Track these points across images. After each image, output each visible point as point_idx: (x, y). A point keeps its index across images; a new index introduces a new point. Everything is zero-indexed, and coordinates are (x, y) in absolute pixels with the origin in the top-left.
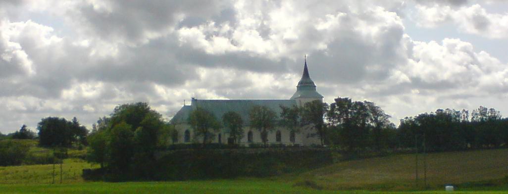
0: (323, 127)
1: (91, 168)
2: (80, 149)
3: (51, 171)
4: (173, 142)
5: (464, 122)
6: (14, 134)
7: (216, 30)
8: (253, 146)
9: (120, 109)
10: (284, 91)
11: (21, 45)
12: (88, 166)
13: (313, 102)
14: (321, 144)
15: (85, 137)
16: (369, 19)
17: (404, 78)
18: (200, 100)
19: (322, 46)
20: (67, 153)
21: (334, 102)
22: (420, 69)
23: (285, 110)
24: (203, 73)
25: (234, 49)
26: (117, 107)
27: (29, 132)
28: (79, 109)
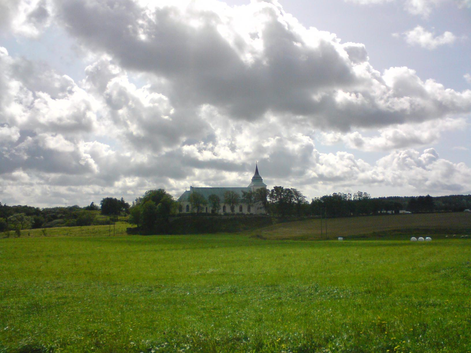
0: (267, 203)
1: (131, 227)
2: (125, 216)
3: (108, 229)
4: (180, 212)
5: (349, 200)
6: (86, 207)
7: (204, 146)
8: (226, 214)
9: (148, 193)
10: (244, 182)
11: (91, 155)
12: (130, 226)
13: (261, 189)
14: (265, 213)
15: (128, 209)
16: (294, 140)
17: (314, 174)
18: (195, 188)
19: (266, 156)
20: (117, 219)
21: (273, 188)
22: (323, 169)
23: (245, 194)
24: (197, 172)
25: (215, 157)
26: (147, 192)
27: (95, 206)
28: (125, 193)
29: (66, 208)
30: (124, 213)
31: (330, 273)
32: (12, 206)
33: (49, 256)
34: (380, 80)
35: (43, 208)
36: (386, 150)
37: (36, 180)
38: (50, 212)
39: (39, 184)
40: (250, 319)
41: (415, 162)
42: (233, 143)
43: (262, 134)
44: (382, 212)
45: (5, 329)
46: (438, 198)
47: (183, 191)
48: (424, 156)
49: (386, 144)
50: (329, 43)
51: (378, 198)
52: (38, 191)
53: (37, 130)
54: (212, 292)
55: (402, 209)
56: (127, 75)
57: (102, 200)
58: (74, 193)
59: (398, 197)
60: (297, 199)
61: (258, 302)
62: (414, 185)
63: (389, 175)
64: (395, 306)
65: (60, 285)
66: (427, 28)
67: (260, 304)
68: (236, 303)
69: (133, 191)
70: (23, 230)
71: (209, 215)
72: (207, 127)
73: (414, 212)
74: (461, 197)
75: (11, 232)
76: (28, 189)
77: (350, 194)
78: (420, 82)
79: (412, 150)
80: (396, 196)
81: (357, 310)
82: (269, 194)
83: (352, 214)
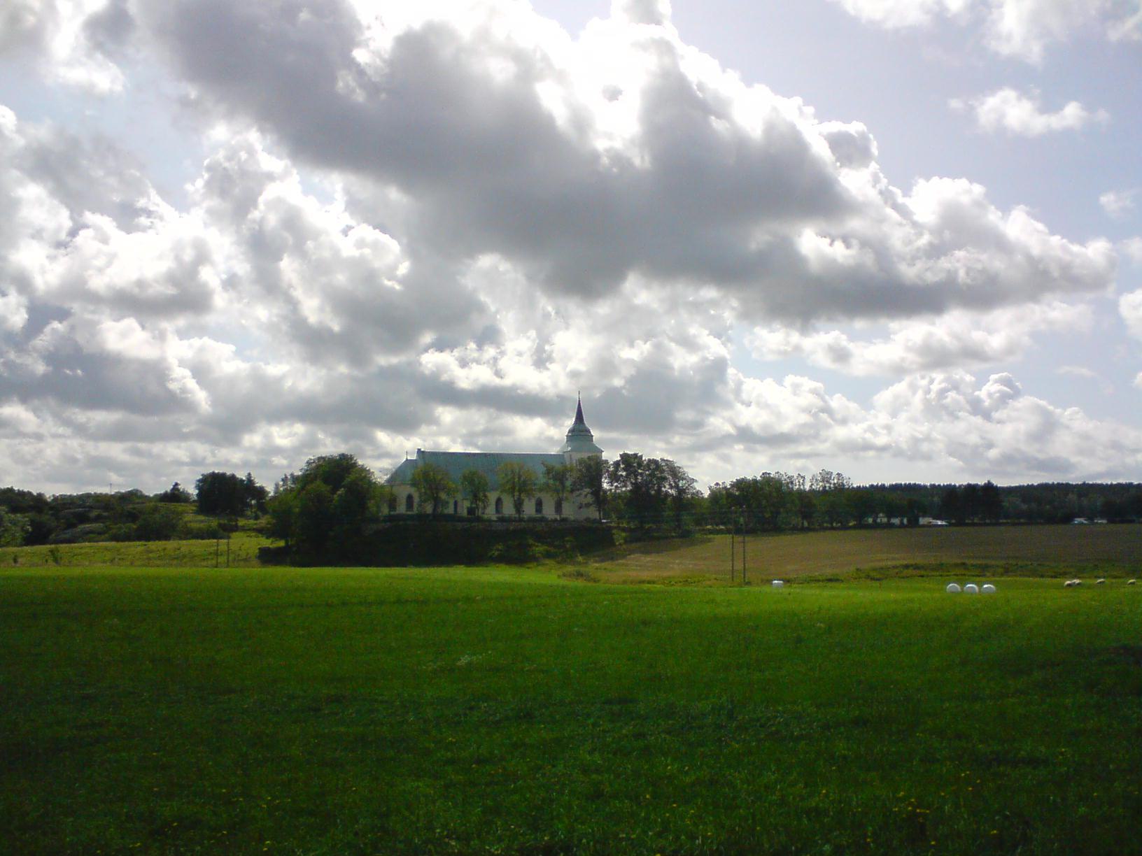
0: (601, 493)
1: (271, 546)
2: (256, 518)
3: (212, 549)
4: (390, 511)
5: (799, 490)
6: (161, 494)
7: (475, 355)
8: (502, 520)
10: (550, 440)
12: (267, 543)
13: (589, 458)
15: (264, 501)
16: (689, 344)
17: (728, 429)
19: (618, 382)
20: (237, 524)
21: (619, 458)
22: (750, 417)
23: (549, 471)
24: (447, 415)
27: (183, 492)
28: (265, 464)
29: (112, 496)
36: (899, 371)
37: (50, 426)
38: (70, 504)
43: (618, 328)
46: (1010, 490)
48: (991, 389)
51: (868, 486)
52: (52, 451)
53: (76, 307)
58: (144, 461)
59: (915, 484)
62: (960, 457)
63: (904, 430)
71: (461, 519)
72: (481, 308)
73: (953, 521)
74: (1065, 488)
76: (27, 448)
78: (993, 216)
79: (963, 375)
80: (912, 482)
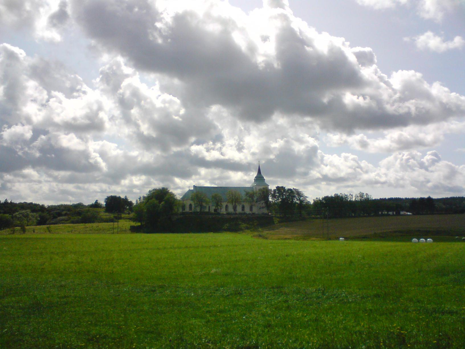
1: (135, 225)
2: (129, 214)
7: (213, 146)
8: (228, 214)
10: (249, 182)
11: (99, 154)
12: (133, 224)
13: (264, 188)
15: (132, 207)
16: (300, 141)
17: (318, 175)
19: (272, 157)
21: (276, 188)
22: (327, 170)
23: (247, 194)
24: (203, 171)
25: (222, 157)
28: (131, 192)
29: (71, 206)
30: (128, 211)
31: (335, 275)
32: (18, 203)
33: (52, 253)
34: (387, 83)
35: (48, 205)
36: (389, 151)
37: (44, 178)
39: (47, 181)
40: (258, 325)
41: (418, 163)
42: (241, 143)
43: (270, 135)
44: (384, 213)
45: (6, 330)
47: (187, 190)
48: (428, 158)
49: (390, 146)
50: (340, 49)
52: (45, 188)
53: (50, 129)
54: (217, 293)
55: (402, 211)
56: (139, 75)
57: (106, 197)
59: (398, 198)
60: (299, 199)
61: (265, 306)
63: (392, 176)
64: (408, 312)
65: (63, 283)
66: (437, 33)
67: (267, 307)
68: (242, 305)
69: (139, 189)
70: (28, 227)
71: (211, 214)
72: (215, 127)
75: (16, 228)
76: (36, 186)
77: (351, 195)
78: (426, 86)
79: (415, 152)
81: (369, 315)
82: (271, 194)
83: (353, 215)
